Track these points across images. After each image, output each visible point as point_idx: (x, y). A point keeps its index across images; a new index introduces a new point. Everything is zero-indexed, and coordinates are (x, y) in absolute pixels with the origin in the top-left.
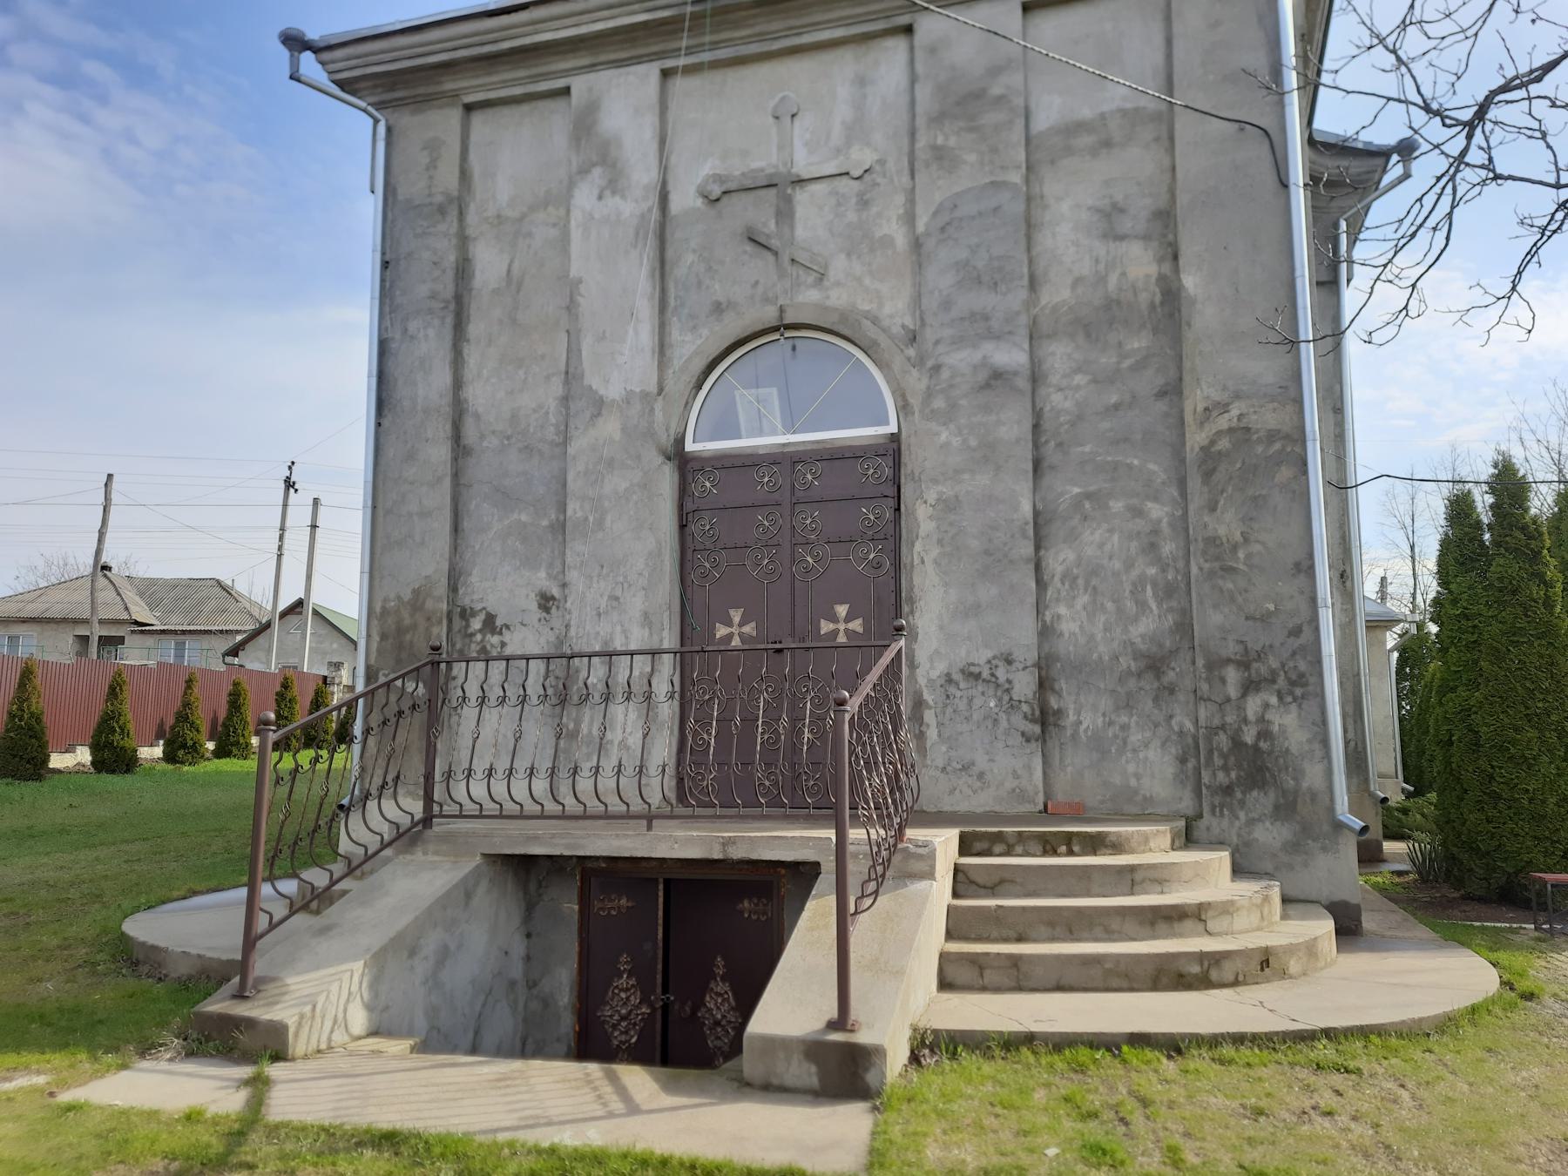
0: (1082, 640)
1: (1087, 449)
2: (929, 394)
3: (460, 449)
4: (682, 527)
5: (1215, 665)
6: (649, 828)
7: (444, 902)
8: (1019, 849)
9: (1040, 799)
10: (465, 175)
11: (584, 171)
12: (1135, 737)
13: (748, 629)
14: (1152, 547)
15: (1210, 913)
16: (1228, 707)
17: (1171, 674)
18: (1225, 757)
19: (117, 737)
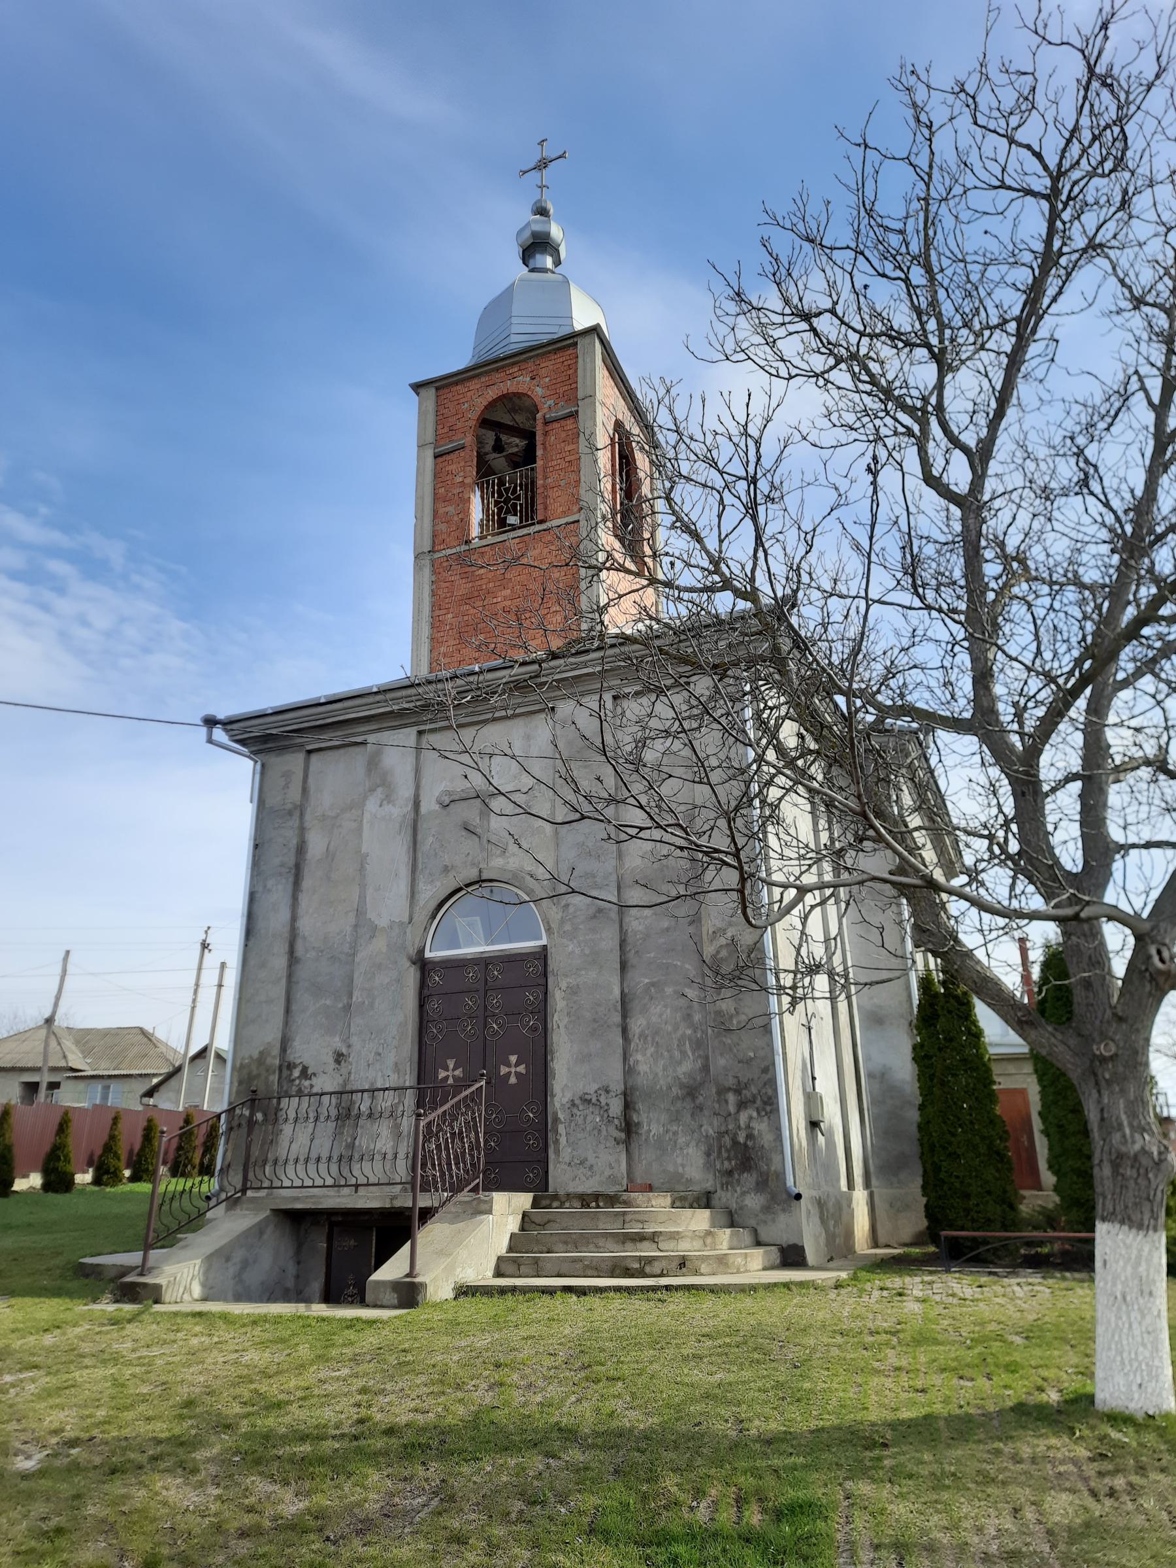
0: (651, 1077)
1: (652, 955)
2: (562, 922)
3: (293, 959)
4: (421, 1006)
5: (722, 1091)
6: (356, 1192)
7: (246, 1234)
8: (567, 1205)
9: (625, 1182)
10: (305, 790)
11: (372, 790)
12: (682, 1140)
13: (458, 1072)
14: (688, 1017)
15: (661, 1238)
16: (729, 1119)
17: (701, 1098)
18: (728, 1151)
19: (61, 1164)
